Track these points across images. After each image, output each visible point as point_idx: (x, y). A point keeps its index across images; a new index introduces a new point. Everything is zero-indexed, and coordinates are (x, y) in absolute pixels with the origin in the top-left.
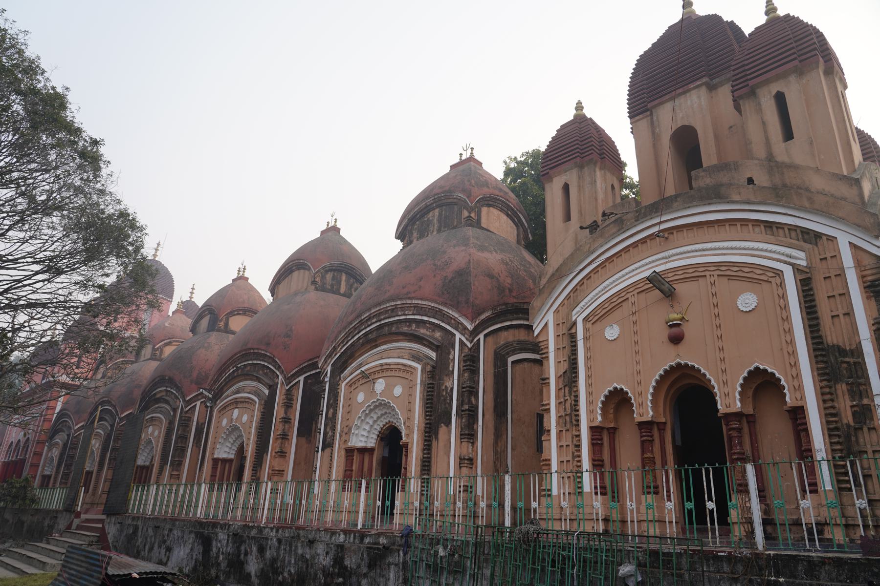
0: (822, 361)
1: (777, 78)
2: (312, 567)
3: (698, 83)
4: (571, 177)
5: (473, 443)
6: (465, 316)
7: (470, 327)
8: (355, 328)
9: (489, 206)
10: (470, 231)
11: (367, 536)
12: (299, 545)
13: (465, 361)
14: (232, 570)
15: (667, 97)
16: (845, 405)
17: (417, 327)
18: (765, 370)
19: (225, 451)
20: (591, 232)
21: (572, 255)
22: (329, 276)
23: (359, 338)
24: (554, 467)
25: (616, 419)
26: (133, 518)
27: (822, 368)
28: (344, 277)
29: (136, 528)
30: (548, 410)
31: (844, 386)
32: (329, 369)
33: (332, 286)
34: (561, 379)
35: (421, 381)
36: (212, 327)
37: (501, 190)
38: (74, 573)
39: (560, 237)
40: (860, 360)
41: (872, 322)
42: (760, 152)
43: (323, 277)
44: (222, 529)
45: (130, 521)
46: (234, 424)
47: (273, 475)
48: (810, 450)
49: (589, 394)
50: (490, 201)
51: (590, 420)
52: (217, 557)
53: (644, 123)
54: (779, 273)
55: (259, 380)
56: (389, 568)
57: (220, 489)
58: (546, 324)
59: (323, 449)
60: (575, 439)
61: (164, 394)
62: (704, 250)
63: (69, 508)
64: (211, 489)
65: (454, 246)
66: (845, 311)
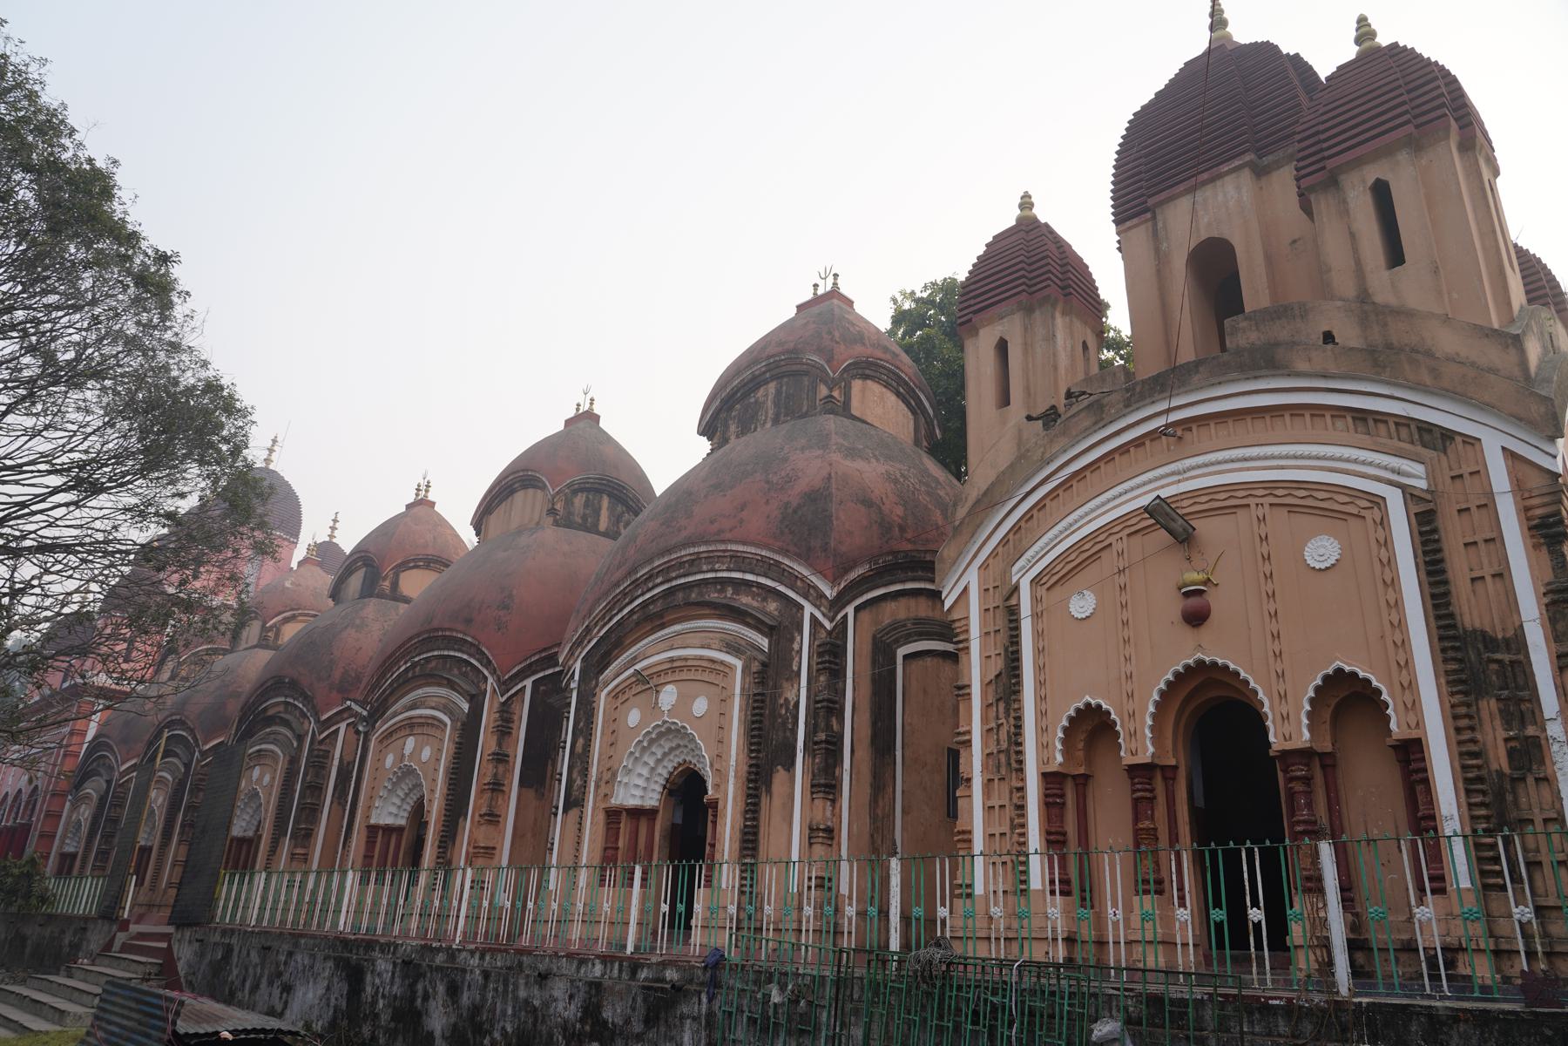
1: (1376, 156)
2: (543, 1021)
3: (1237, 163)
4: (1010, 327)
5: (833, 801)
6: (822, 574)
7: (830, 593)
8: (624, 594)
9: (865, 377)
10: (831, 423)
11: (642, 966)
12: (522, 981)
13: (820, 655)
15: (1181, 187)
16: (1495, 738)
17: (736, 592)
18: (1354, 674)
19: (389, 812)
20: (1046, 426)
21: (1012, 466)
22: (579, 500)
24: (978, 844)
25: (1089, 760)
26: (224, 932)
27: (1455, 672)
29: (229, 950)
30: (968, 743)
31: (1493, 702)
32: (578, 666)
33: (584, 517)
34: (992, 688)
35: (743, 689)
36: (370, 590)
37: (886, 350)
39: (991, 434)
40: (1521, 657)
41: (1543, 590)
42: (1345, 285)
43: (569, 503)
44: (382, 952)
45: (217, 938)
46: (407, 764)
47: (476, 855)
48: (1433, 817)
49: (1041, 714)
50: (867, 369)
51: (1043, 761)
52: (374, 1002)
53: (1141, 234)
54: (1378, 502)
55: (452, 685)
56: (682, 1025)
57: (380, 881)
58: (966, 589)
59: (565, 811)
60: (1016, 795)
61: (281, 708)
62: (1246, 460)
63: (109, 912)
66: (1496, 569)
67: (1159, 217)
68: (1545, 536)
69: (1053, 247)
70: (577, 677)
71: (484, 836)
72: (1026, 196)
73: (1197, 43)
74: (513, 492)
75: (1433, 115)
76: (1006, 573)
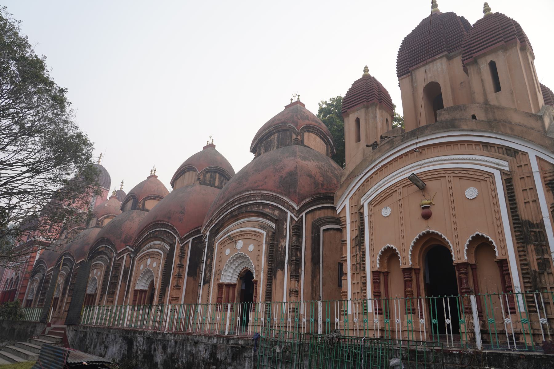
0: (519, 231)
1: (491, 52)
2: (196, 359)
3: (441, 55)
4: (360, 114)
5: (298, 281)
6: (294, 201)
7: (297, 208)
8: (224, 208)
9: (309, 132)
10: (297, 148)
11: (231, 339)
12: (188, 345)
13: (293, 229)
14: (146, 360)
15: (421, 64)
16: (533, 259)
17: (264, 207)
18: (483, 236)
19: (142, 285)
20: (373, 149)
21: (361, 163)
22: (208, 175)
23: (227, 215)
24: (349, 296)
26: (84, 327)
27: (519, 235)
28: (217, 176)
29: (86, 333)
30: (346, 261)
31: (532, 246)
32: (208, 234)
33: (210, 181)
34: (354, 241)
35: (266, 242)
38: (46, 361)
39: (354, 152)
40: (542, 230)
41: (550, 206)
42: (479, 98)
43: (204, 176)
44: (140, 334)
45: (82, 329)
46: (148, 268)
47: (172, 300)
48: (511, 287)
49: (372, 250)
50: (310, 129)
51: (372, 267)
52: (137, 352)
53: (407, 80)
54: (491, 175)
55: (163, 240)
56: (245, 360)
57: (139, 309)
58: (345, 206)
59: (204, 285)
60: (363, 279)
61: (104, 249)
62: (444, 160)
63: (44, 320)
64: (133, 309)
65: (287, 157)
66: (533, 199)
67: (413, 75)
68: (551, 187)
69: (376, 85)
70: (207, 238)
71: (175, 293)
72: (366, 67)
73: (427, 13)
74: (185, 172)
75: (511, 38)
76: (359, 200)
